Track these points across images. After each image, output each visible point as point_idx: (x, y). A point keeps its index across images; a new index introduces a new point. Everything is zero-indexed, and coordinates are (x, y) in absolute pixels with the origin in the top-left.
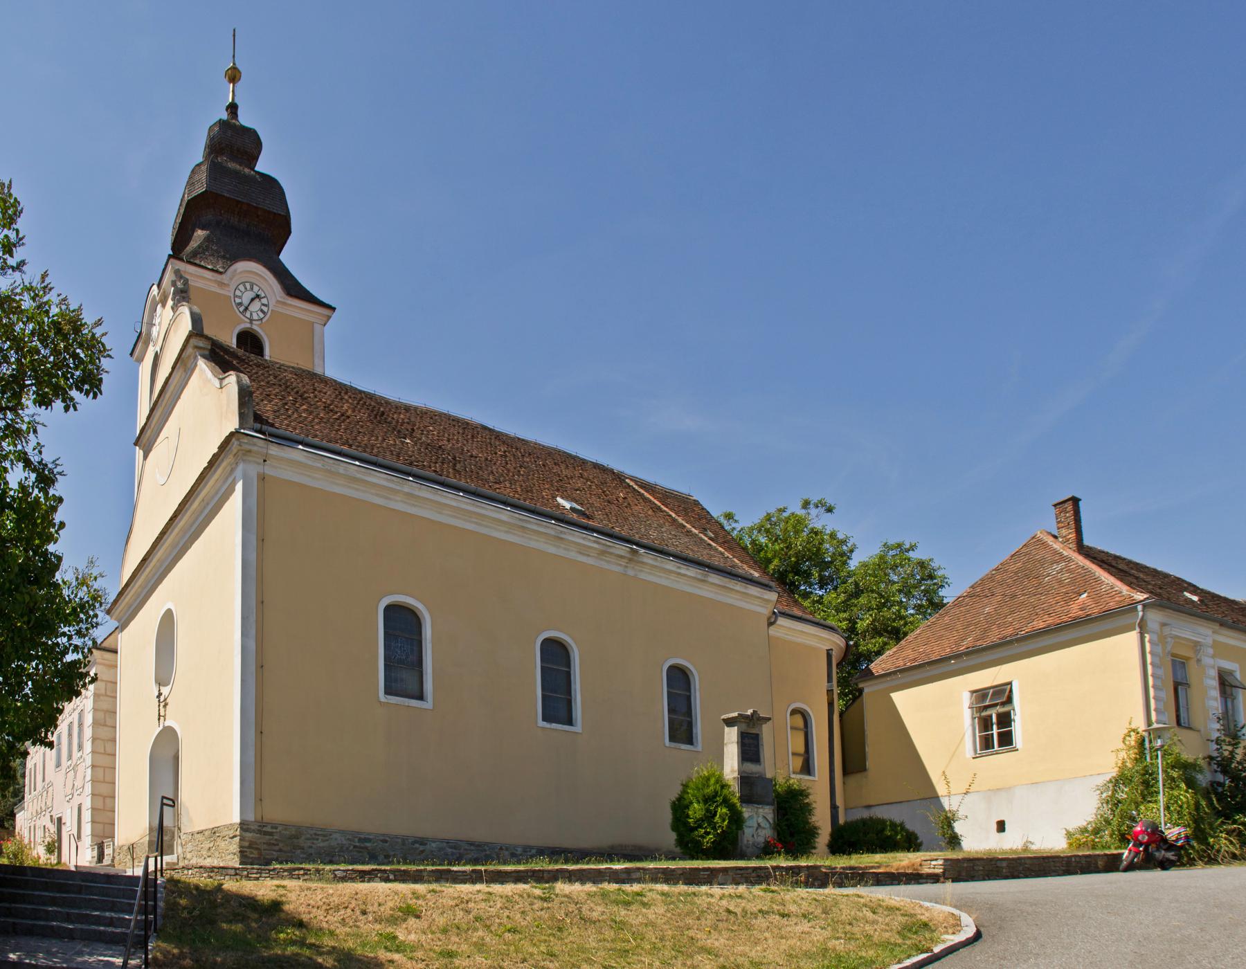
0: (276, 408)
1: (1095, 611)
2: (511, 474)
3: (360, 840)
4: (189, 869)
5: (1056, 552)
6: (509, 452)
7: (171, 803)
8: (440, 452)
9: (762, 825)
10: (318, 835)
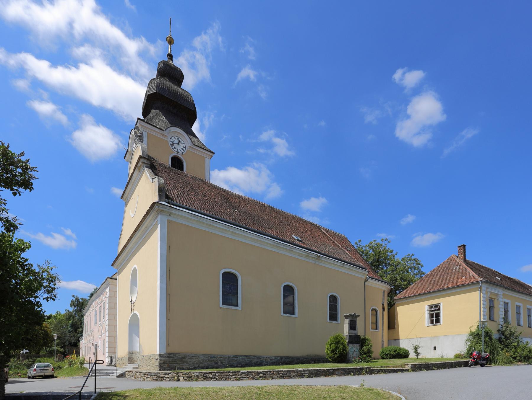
0: (179, 193)
1: (467, 283)
2: (276, 225)
3: (211, 357)
4: (137, 373)
5: (457, 262)
6: (278, 216)
7: (102, 362)
8: (249, 215)
9: (355, 350)
10: (194, 357)
